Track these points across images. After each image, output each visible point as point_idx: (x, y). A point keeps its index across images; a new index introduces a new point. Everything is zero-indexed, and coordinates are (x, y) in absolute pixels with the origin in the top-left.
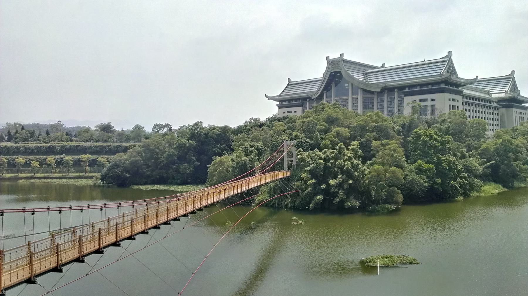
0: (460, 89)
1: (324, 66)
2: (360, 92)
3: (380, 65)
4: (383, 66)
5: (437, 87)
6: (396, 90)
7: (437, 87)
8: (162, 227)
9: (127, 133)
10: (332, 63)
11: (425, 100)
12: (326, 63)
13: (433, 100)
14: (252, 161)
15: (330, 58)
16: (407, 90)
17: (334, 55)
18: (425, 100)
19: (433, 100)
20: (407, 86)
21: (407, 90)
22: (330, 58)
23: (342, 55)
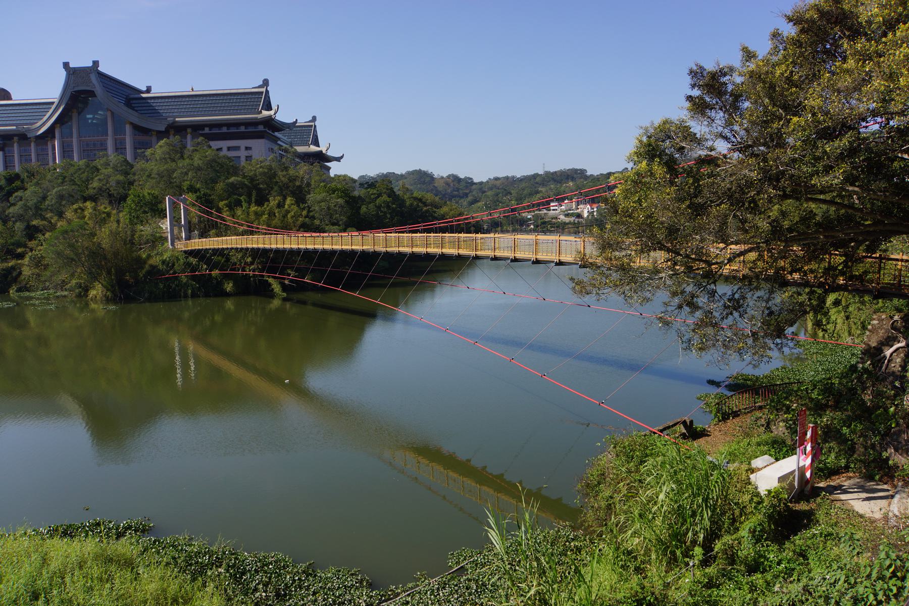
0: (276, 134)
1: (61, 77)
2: (128, 128)
3: (145, 89)
4: (149, 90)
5: (251, 129)
6: (189, 130)
7: (251, 129)
8: (672, 334)
9: (440, 185)
10: (73, 73)
11: (237, 148)
12: (63, 74)
13: (247, 148)
14: (896, 216)
15: (71, 66)
16: (207, 130)
17: (81, 61)
18: (237, 148)
19: (247, 148)
20: (206, 126)
21: (207, 130)
22: (71, 66)
23: (96, 63)
